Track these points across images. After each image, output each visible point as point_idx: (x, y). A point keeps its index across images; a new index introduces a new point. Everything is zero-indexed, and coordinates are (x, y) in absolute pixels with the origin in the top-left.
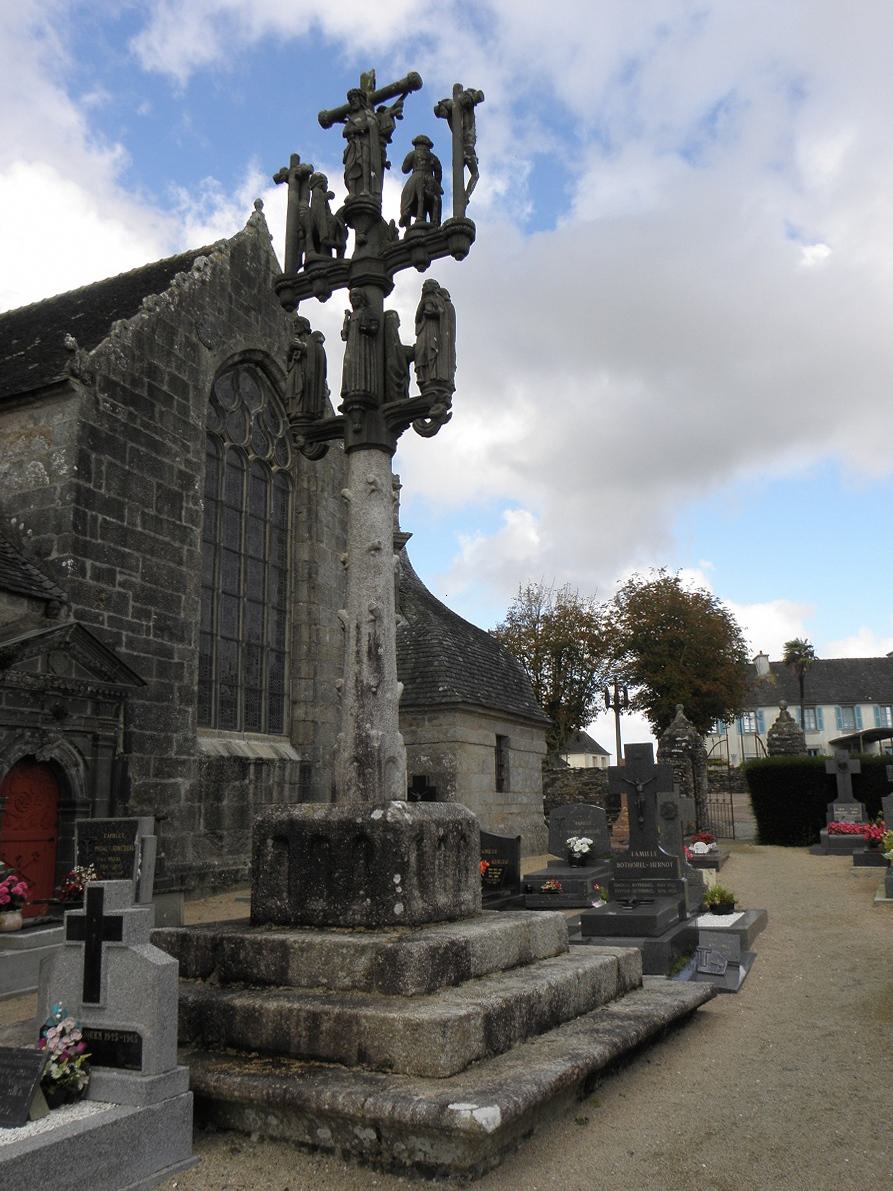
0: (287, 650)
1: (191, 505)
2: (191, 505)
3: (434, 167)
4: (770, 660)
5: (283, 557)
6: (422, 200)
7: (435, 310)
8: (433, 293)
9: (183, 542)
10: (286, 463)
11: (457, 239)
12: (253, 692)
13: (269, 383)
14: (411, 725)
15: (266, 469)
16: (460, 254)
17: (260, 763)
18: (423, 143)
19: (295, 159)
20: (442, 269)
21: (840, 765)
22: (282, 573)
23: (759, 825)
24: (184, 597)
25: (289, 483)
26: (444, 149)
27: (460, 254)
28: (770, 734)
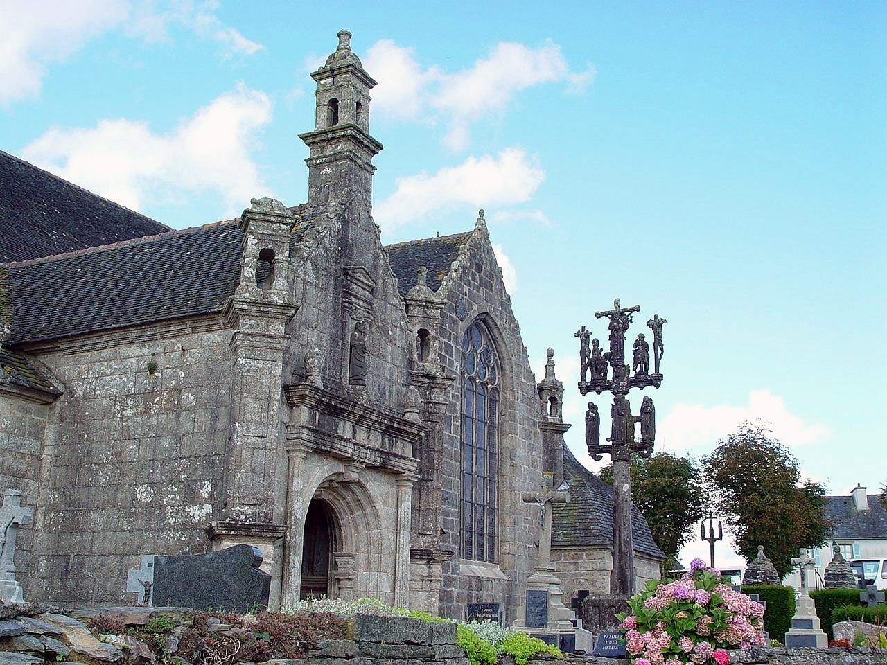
0: (496, 507)
1: (455, 423)
2: (455, 423)
3: (646, 347)
4: (869, 492)
5: (492, 445)
6: (641, 359)
7: (648, 409)
8: (647, 402)
9: (452, 446)
10: (495, 383)
11: (656, 381)
12: (480, 535)
13: (487, 331)
14: (574, 558)
15: (485, 387)
16: (658, 386)
17: (488, 579)
18: (641, 337)
19: (583, 328)
20: (649, 391)
21: (870, 596)
22: (493, 455)
23: (191, 238)
24: (453, 479)
25: (497, 394)
26: (650, 339)
27: (658, 386)
28: (826, 571)
